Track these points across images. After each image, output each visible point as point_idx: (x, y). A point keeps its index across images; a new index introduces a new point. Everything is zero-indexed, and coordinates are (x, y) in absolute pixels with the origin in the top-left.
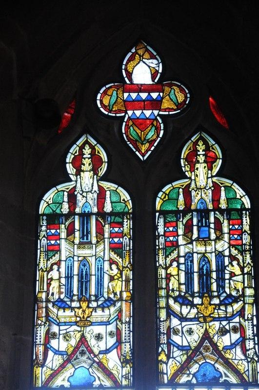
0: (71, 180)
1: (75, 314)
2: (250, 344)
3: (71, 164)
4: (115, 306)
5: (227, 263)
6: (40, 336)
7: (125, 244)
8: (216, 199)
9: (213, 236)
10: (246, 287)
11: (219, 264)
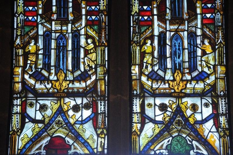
1: (169, 87)
2: (222, 119)
4: (90, 79)
5: (199, 41)
6: (136, 105)
9: (71, 17)
10: (217, 65)
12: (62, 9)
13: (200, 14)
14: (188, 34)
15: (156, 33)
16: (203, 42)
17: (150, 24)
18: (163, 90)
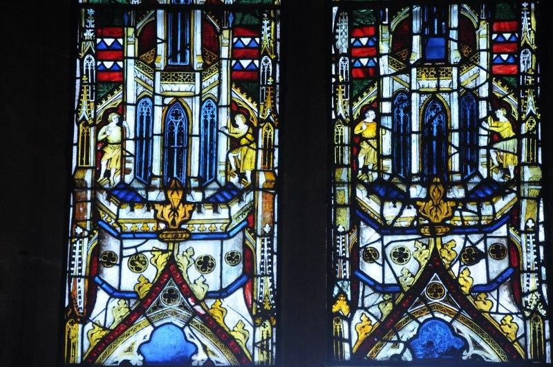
4: (241, 200)
5: (483, 113)
6: (80, 259)
9: (455, 57)
10: (524, 164)
12: (179, 49)
13: (228, 59)
14: (459, 98)
15: (131, 98)
16: (492, 114)
17: (373, 76)
18: (210, 225)
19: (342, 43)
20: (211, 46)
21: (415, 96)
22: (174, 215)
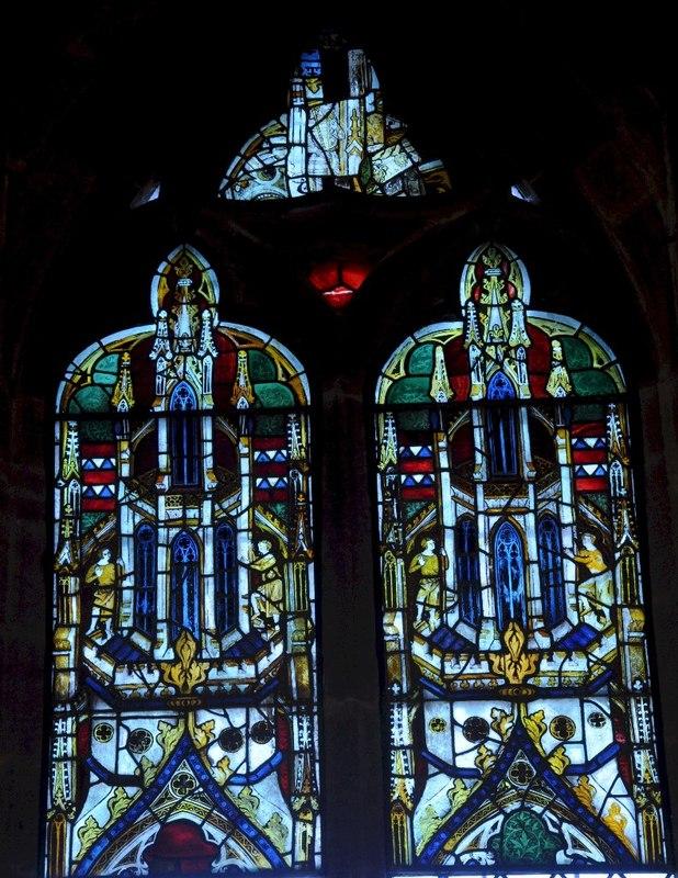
0: (149, 319)
3: (164, 279)
5: (567, 541)
7: (614, 477)
8: (223, 382)
9: (210, 483)
10: (622, 606)
11: (142, 561)
12: (185, 461)
19: (389, 452)
20: (544, 447)
21: (481, 519)
22: (185, 676)
